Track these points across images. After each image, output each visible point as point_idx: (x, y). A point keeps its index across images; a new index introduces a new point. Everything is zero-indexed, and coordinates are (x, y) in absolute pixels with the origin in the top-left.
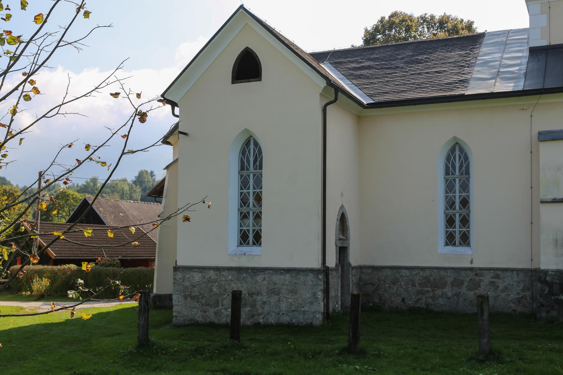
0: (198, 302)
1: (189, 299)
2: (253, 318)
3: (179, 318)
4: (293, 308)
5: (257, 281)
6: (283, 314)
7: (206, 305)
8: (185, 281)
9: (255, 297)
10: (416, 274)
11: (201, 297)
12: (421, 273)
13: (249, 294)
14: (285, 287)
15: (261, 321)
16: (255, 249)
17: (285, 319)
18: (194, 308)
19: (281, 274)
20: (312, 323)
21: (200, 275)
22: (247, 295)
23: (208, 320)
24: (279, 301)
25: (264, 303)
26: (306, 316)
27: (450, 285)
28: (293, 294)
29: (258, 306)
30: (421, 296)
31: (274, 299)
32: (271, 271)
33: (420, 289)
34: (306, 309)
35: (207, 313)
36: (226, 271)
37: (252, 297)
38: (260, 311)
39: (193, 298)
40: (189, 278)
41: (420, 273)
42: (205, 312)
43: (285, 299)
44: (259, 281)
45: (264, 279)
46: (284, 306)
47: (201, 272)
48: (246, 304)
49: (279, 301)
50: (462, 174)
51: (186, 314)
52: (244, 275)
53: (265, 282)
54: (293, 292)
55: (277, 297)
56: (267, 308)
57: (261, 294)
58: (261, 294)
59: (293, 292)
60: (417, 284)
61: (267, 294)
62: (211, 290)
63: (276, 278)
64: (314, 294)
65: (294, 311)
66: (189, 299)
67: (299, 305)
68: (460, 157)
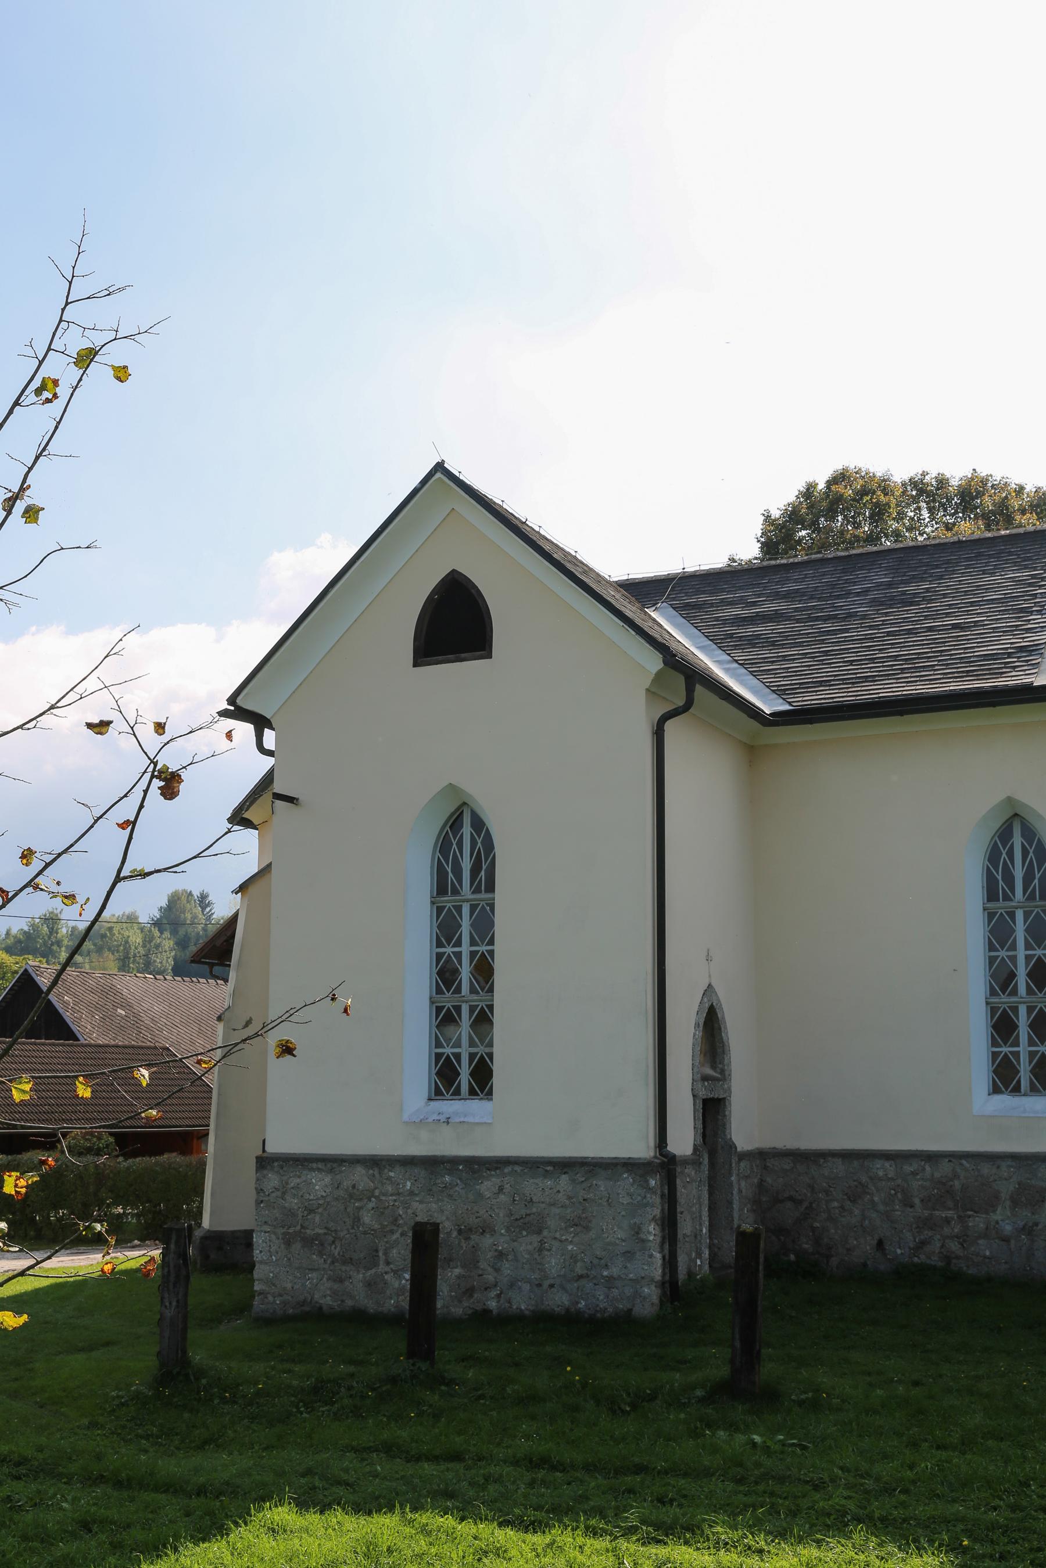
0: (321, 1254)
1: (297, 1247)
2: (471, 1296)
3: (271, 1298)
4: (579, 1269)
5: (480, 1195)
6: (552, 1286)
7: (344, 1263)
8: (287, 1197)
9: (474, 1237)
10: (914, 1174)
11: (331, 1239)
12: (928, 1168)
13: (460, 1232)
14: (558, 1211)
15: (493, 1305)
16: (475, 1109)
17: (558, 1300)
18: (312, 1270)
19: (546, 1174)
20: (630, 1310)
21: (328, 1179)
22: (455, 1234)
23: (349, 1303)
24: (540, 1250)
25: (501, 1255)
26: (615, 1292)
27: (1008, 1203)
28: (579, 1229)
29: (483, 1265)
30: (927, 1233)
31: (527, 1244)
32: (518, 1168)
33: (926, 1213)
34: (615, 1271)
35: (347, 1283)
36: (398, 1168)
37: (467, 1239)
38: (490, 1278)
39: (308, 1242)
40: (297, 1187)
41: (924, 1169)
42: (341, 1281)
43: (556, 1244)
44: (488, 1194)
45: (501, 1189)
46: (553, 1264)
47: (331, 1171)
48: (451, 1260)
49: (540, 1250)
50: (1031, 898)
51: (289, 1286)
52: (447, 1178)
53: (502, 1196)
54: (580, 1224)
55: (535, 1239)
56: (507, 1268)
57: (493, 1232)
58: (493, 1232)
59: (580, 1224)
60: (917, 1201)
61: (508, 1229)
62: (357, 1220)
63: (534, 1187)
64: (637, 1230)
65: (581, 1277)
66: (297, 1247)
67: (596, 1261)
68: (1025, 853)
